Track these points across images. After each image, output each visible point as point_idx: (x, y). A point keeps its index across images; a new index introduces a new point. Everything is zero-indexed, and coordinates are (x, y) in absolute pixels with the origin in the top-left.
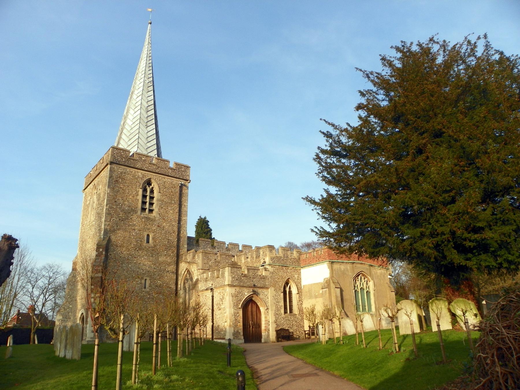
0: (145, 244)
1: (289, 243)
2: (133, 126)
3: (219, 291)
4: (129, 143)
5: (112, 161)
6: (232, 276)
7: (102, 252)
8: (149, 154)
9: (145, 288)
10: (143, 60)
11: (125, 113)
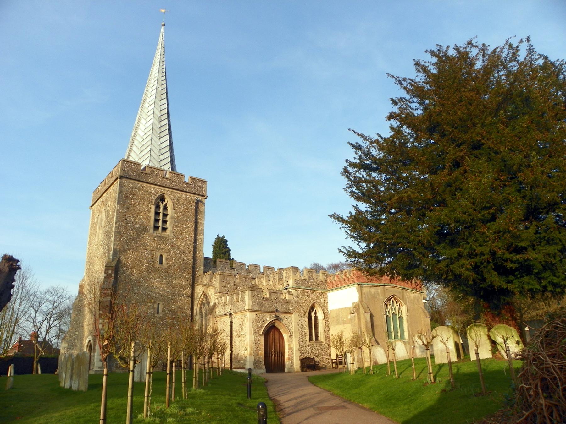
0: (158, 265)
1: (315, 264)
2: (144, 137)
3: (238, 317)
4: (141, 156)
5: (122, 175)
6: (252, 300)
7: (111, 274)
8: (162, 168)
9: (158, 313)
10: (156, 66)
11: (136, 123)
